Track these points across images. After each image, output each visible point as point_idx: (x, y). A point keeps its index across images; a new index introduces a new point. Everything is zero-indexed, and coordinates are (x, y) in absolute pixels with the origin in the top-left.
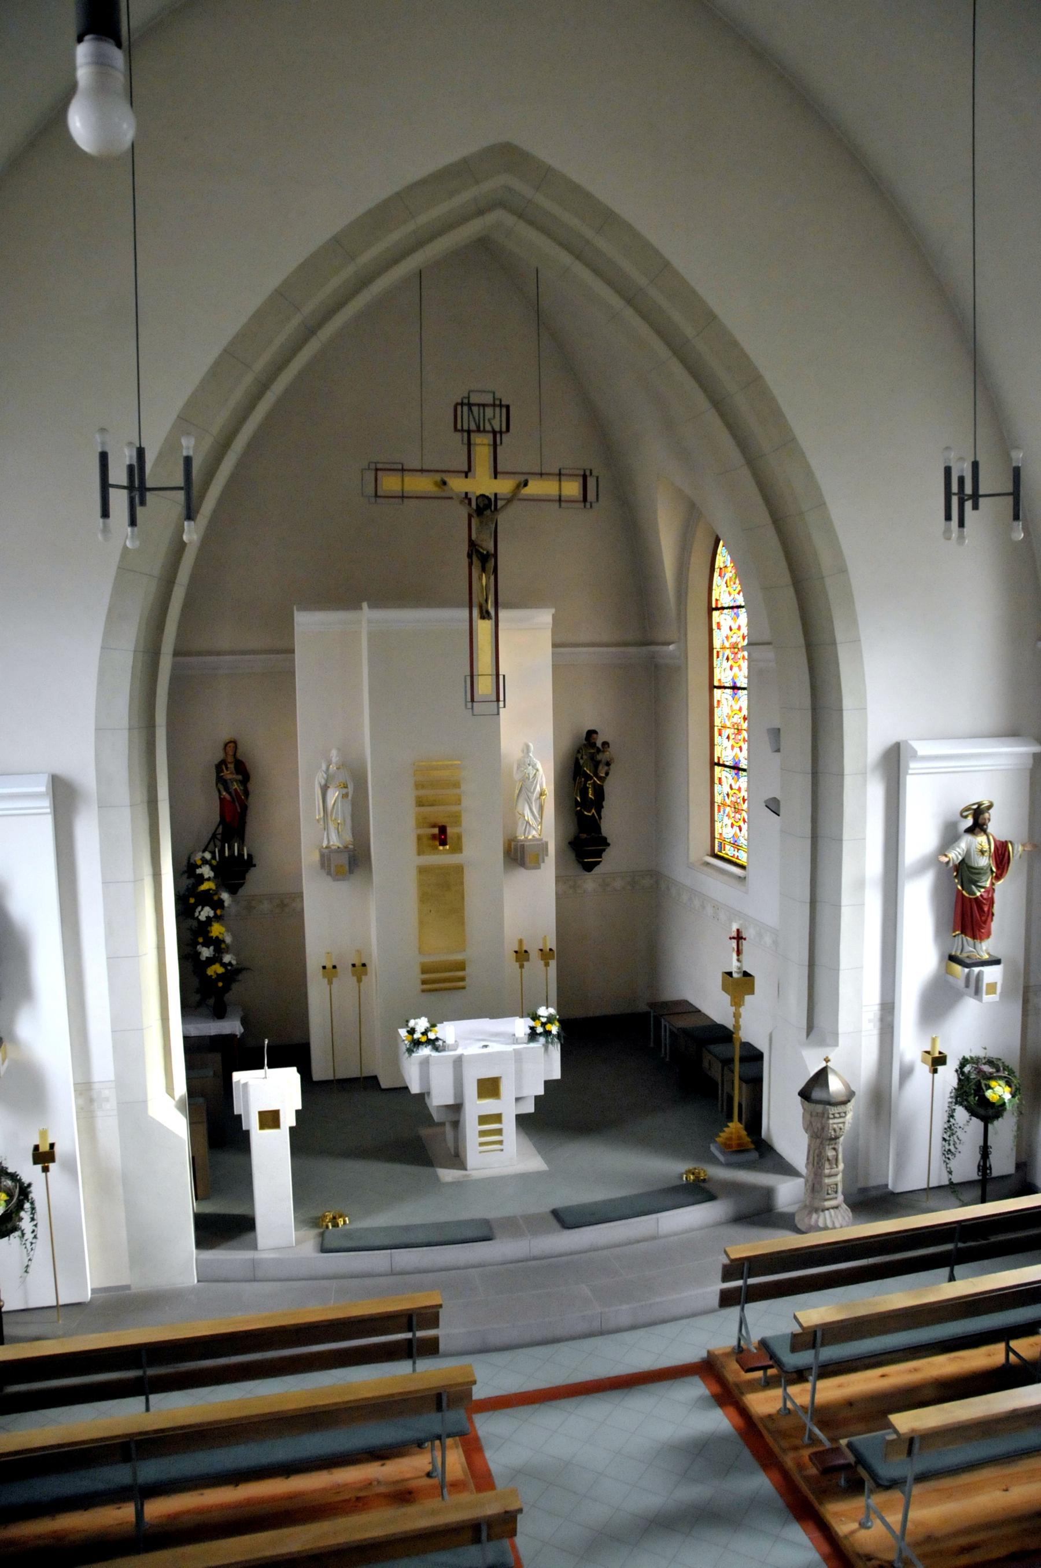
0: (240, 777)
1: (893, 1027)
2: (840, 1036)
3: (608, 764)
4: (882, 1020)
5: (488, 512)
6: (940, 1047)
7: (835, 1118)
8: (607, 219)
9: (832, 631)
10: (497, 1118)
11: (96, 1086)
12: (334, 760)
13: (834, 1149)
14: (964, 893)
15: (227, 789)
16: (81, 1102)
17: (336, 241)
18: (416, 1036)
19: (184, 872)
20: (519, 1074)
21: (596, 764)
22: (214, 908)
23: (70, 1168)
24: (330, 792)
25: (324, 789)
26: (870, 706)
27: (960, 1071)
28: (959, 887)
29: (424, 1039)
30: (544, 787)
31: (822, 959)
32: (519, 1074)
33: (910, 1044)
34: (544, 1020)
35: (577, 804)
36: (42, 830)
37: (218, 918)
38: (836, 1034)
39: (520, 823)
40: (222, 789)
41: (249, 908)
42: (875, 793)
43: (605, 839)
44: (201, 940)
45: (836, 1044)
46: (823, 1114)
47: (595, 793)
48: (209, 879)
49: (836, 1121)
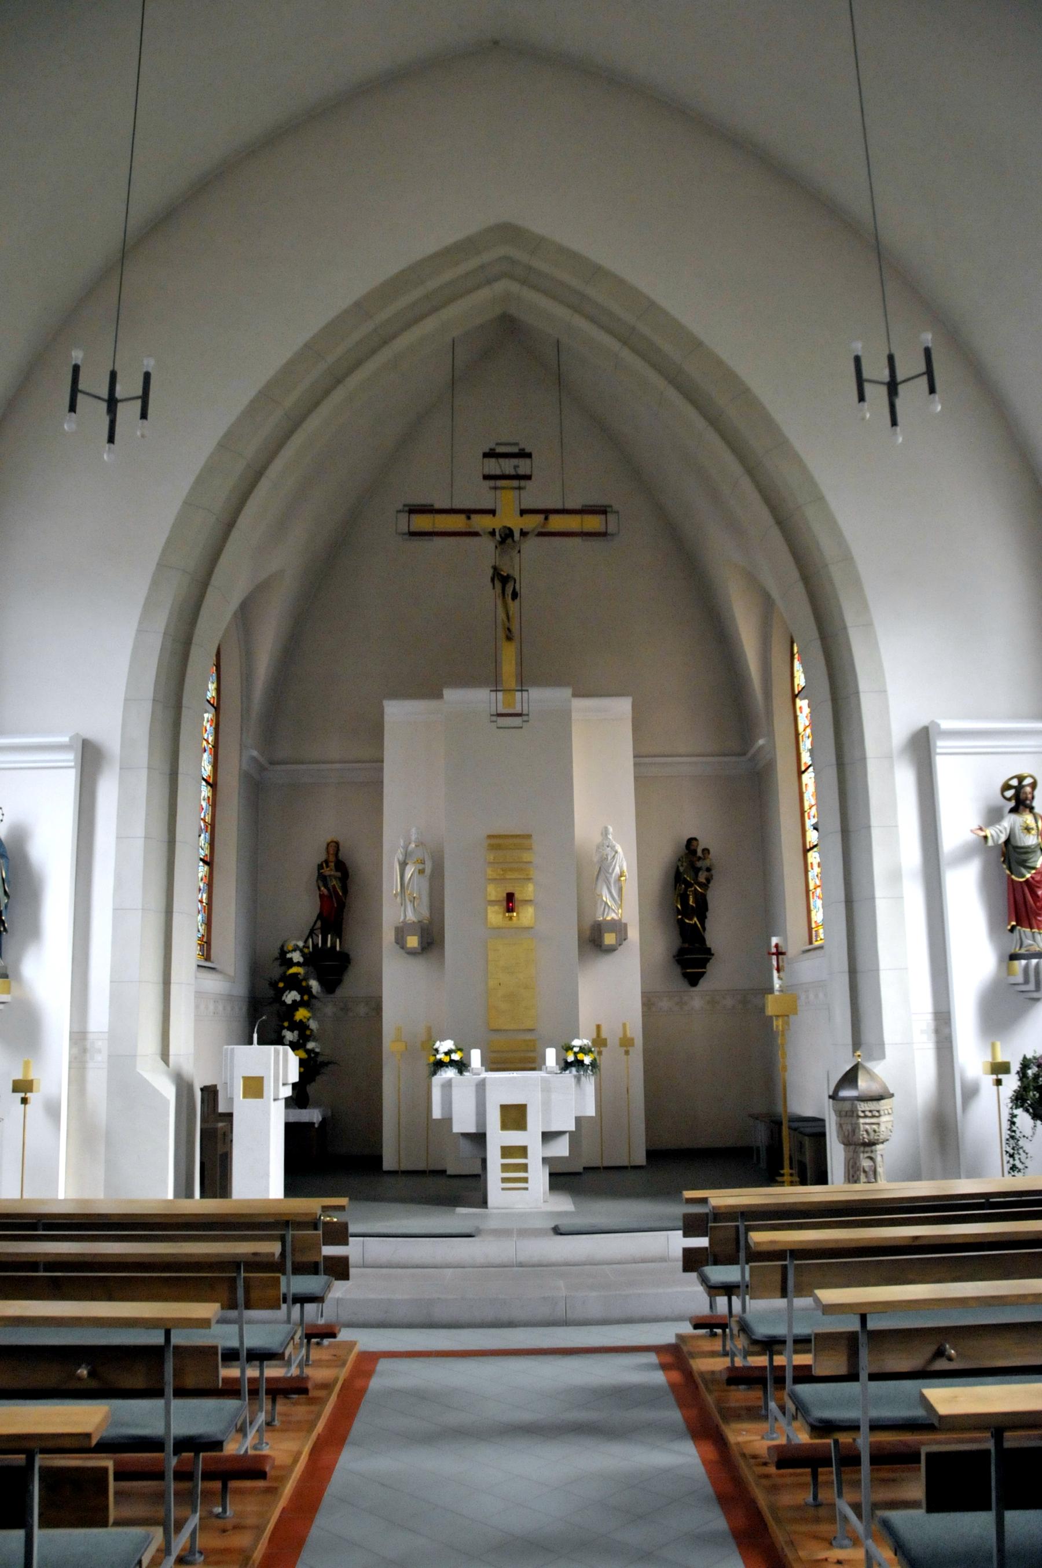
0: (339, 874)
1: (951, 1042)
2: (886, 1046)
3: (709, 870)
4: (937, 1031)
5: (509, 541)
6: (1000, 1058)
7: (866, 1117)
8: (597, 272)
9: (843, 620)
10: (523, 1151)
11: (91, 1037)
12: (413, 838)
13: (871, 1158)
14: (1013, 877)
15: (326, 886)
16: (75, 1051)
17: (357, 305)
18: (438, 1057)
19: (276, 959)
20: (546, 1105)
21: (697, 871)
22: (302, 994)
23: (53, 1111)
24: (408, 867)
25: (403, 865)
26: (890, 689)
27: (1022, 1074)
28: (1008, 872)
29: (446, 1059)
30: (625, 869)
31: (862, 964)
32: (546, 1105)
33: (972, 1058)
34: (576, 1049)
35: (679, 912)
36: (67, 781)
37: (302, 1004)
38: (881, 1044)
39: (599, 902)
40: (321, 884)
41: (345, 1009)
42: (905, 779)
43: (709, 949)
44: (286, 1024)
45: (882, 1056)
46: (852, 1112)
47: (696, 901)
48: (298, 964)
49: (868, 1120)
